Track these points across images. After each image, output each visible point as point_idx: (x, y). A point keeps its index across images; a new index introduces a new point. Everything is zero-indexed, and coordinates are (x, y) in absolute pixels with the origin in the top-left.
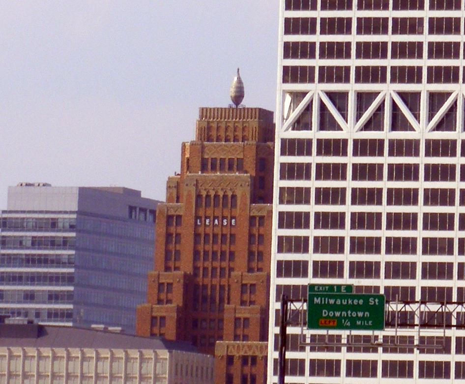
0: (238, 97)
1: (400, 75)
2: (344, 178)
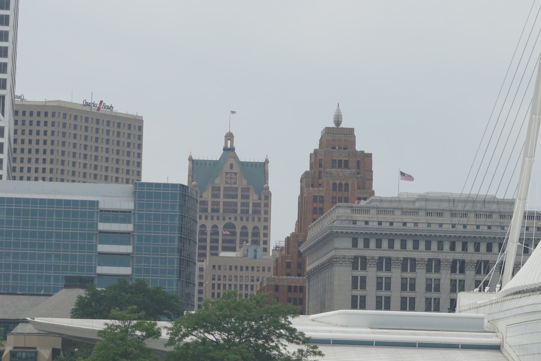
0: (338, 122)
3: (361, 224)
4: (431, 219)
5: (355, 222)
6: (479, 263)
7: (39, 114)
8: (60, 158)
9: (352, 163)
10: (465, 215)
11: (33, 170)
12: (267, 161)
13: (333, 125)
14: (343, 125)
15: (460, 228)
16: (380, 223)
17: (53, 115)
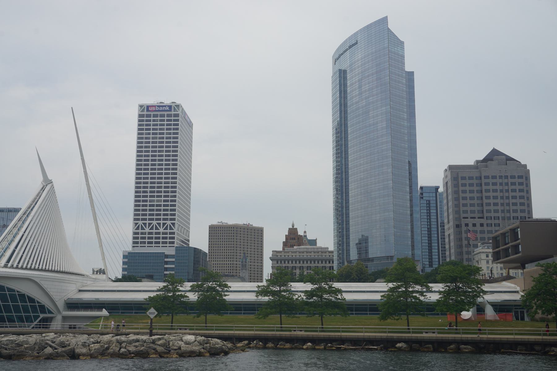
0: (293, 226)
1: (157, 219)
2: (162, 237)
3: (279, 256)
4: (300, 254)
5: (277, 256)
6: (300, 267)
7: (218, 228)
8: (236, 240)
9: (296, 239)
10: (311, 252)
11: (226, 244)
12: (316, 239)
13: (292, 227)
14: (294, 227)
15: (309, 256)
16: (285, 256)
17: (233, 228)
